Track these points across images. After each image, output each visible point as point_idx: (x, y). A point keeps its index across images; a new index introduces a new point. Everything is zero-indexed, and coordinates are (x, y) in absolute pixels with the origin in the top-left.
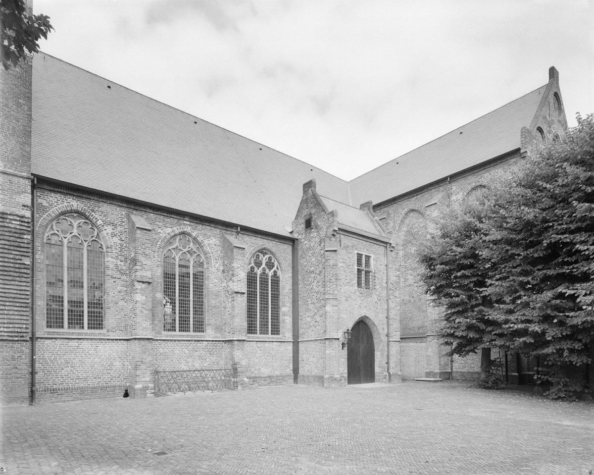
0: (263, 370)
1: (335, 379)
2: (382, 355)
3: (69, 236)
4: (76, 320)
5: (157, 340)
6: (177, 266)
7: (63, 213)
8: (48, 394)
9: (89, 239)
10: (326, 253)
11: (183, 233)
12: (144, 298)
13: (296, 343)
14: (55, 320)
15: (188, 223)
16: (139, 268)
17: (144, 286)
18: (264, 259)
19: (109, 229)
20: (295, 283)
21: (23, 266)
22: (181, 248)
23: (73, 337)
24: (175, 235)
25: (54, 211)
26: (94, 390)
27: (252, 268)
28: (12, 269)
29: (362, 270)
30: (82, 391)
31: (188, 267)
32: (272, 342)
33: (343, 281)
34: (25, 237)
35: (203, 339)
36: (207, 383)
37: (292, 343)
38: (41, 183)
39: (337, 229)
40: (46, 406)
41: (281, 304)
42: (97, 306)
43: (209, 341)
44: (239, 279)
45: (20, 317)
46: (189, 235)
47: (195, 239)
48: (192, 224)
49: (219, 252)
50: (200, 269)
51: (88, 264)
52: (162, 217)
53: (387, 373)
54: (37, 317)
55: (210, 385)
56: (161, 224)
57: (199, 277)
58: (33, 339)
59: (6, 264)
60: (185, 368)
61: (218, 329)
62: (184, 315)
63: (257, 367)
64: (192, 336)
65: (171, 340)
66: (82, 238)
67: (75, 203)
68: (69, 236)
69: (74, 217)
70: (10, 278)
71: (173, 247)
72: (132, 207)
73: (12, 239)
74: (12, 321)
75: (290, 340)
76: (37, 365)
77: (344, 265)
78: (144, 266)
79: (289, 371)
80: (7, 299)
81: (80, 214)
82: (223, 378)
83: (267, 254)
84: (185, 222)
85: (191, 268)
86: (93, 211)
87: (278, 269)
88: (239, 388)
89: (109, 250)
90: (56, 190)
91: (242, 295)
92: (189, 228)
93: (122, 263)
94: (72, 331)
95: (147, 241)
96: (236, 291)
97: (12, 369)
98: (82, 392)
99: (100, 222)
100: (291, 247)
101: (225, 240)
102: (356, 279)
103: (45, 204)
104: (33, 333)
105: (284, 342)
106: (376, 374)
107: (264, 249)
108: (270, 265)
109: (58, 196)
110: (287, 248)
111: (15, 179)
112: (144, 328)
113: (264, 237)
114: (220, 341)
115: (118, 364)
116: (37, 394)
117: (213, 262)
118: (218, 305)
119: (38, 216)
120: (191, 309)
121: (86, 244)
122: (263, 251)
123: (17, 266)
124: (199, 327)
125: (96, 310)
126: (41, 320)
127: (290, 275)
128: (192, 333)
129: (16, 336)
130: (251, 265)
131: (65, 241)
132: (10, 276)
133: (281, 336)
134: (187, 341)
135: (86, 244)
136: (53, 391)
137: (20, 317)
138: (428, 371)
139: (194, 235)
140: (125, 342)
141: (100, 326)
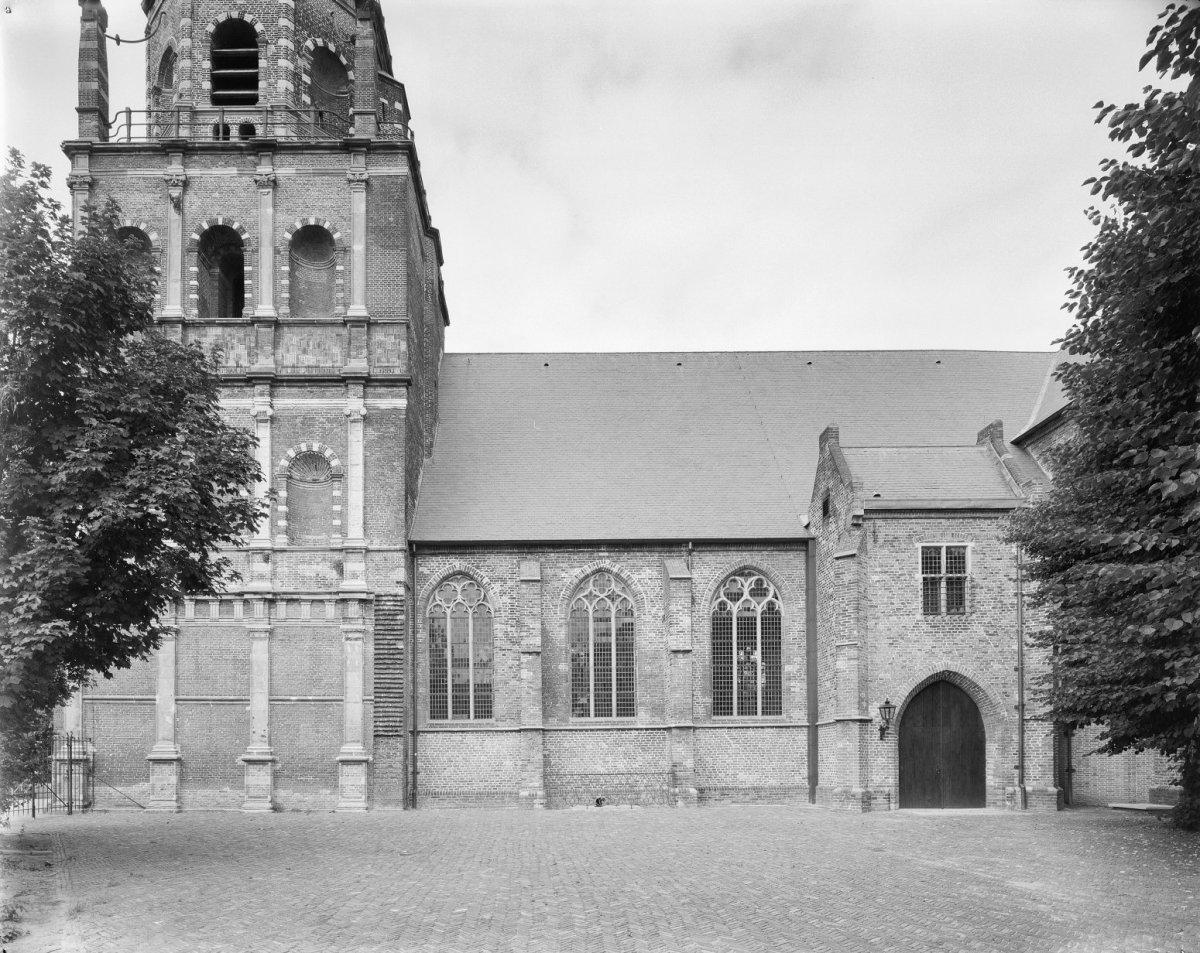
0: (742, 776)
1: (853, 796)
2: (1003, 749)
3: (452, 605)
4: (461, 709)
7: (446, 578)
8: (430, 799)
9: (475, 604)
10: (838, 562)
11: (599, 571)
13: (813, 729)
14: (438, 711)
15: (606, 554)
16: (525, 634)
18: (747, 585)
19: (497, 587)
20: (811, 620)
22: (597, 593)
23: (456, 729)
24: (587, 576)
25: (434, 579)
26: (479, 796)
27: (722, 605)
28: (386, 656)
29: (941, 578)
30: (466, 797)
31: (608, 620)
32: (762, 727)
33: (881, 608)
34: (398, 618)
35: (632, 727)
36: (638, 793)
37: (805, 730)
38: (418, 550)
39: (862, 513)
40: (428, 812)
41: (783, 659)
42: (485, 691)
43: (641, 729)
44: (681, 629)
45: (394, 710)
46: (609, 571)
47: (617, 576)
48: (612, 554)
49: (658, 589)
50: (628, 620)
51: (474, 636)
52: (566, 555)
53: (1018, 789)
54: (419, 708)
55: (643, 796)
57: (626, 631)
58: (415, 733)
59: (381, 652)
60: (602, 770)
61: (658, 710)
63: (730, 772)
64: (614, 723)
65: (581, 730)
66: (467, 604)
67: (457, 563)
68: (452, 605)
69: (458, 580)
70: (385, 666)
71: (586, 593)
74: (386, 714)
76: (419, 764)
77: (885, 577)
78: (532, 631)
79: (801, 778)
80: (382, 690)
81: (464, 575)
82: (665, 787)
83: (754, 575)
84: (601, 554)
85: (613, 620)
86: (478, 567)
87: (777, 598)
88: (680, 803)
89: (497, 614)
90: (437, 552)
91: (686, 655)
92: (608, 561)
93: (513, 629)
95: (536, 596)
96: (675, 648)
97: (387, 768)
98: (466, 798)
99: (486, 580)
100: (803, 553)
101: (664, 570)
102: (921, 599)
103: (426, 571)
104: (415, 726)
105: (788, 727)
106: (989, 790)
107: (745, 568)
108: (759, 591)
109: (439, 558)
110: (795, 561)
111: (389, 554)
112: (531, 715)
113: (744, 548)
114: (659, 729)
115: (508, 763)
116: (418, 797)
117: (647, 606)
118: (656, 672)
119: (419, 587)
120: (614, 682)
121: (470, 611)
122: (743, 572)
123: (391, 652)
124: (627, 708)
126: (424, 709)
127: (802, 604)
128: (614, 718)
129: (391, 731)
130: (719, 600)
131: (448, 611)
132: (385, 664)
133: (784, 716)
135: (470, 611)
136: (435, 795)
137: (394, 710)
138: (1156, 787)
139: (615, 570)
140: (517, 734)
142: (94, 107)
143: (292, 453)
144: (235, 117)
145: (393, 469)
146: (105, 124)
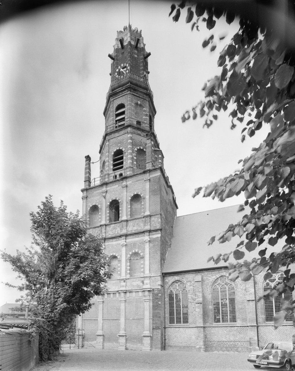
3: (175, 290)
5: (210, 327)
6: (220, 292)
7: (173, 282)
11: (222, 276)
12: (199, 310)
15: (224, 271)
17: (199, 305)
21: (158, 305)
22: (222, 283)
24: (218, 278)
25: (170, 283)
26: (184, 347)
30: (180, 347)
46: (225, 276)
52: (211, 272)
54: (166, 320)
56: (210, 275)
58: (165, 328)
60: (225, 340)
61: (244, 320)
62: (271, 313)
64: (229, 324)
65: (217, 327)
67: (176, 278)
71: (218, 283)
72: (197, 272)
73: (156, 296)
75: (201, 326)
81: (179, 281)
84: (222, 271)
86: (183, 278)
89: (189, 292)
92: (224, 273)
93: (194, 296)
94: (223, 323)
96: (249, 300)
99: (185, 282)
103: (167, 281)
109: (171, 277)
118: (243, 307)
121: (181, 292)
124: (234, 319)
125: (185, 316)
126: (167, 321)
132: (155, 308)
134: (225, 327)
140: (196, 328)
141: (187, 322)
142: (88, 180)
143: (131, 253)
144: (118, 173)
145: (157, 254)
146: (90, 182)
